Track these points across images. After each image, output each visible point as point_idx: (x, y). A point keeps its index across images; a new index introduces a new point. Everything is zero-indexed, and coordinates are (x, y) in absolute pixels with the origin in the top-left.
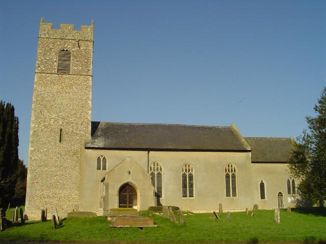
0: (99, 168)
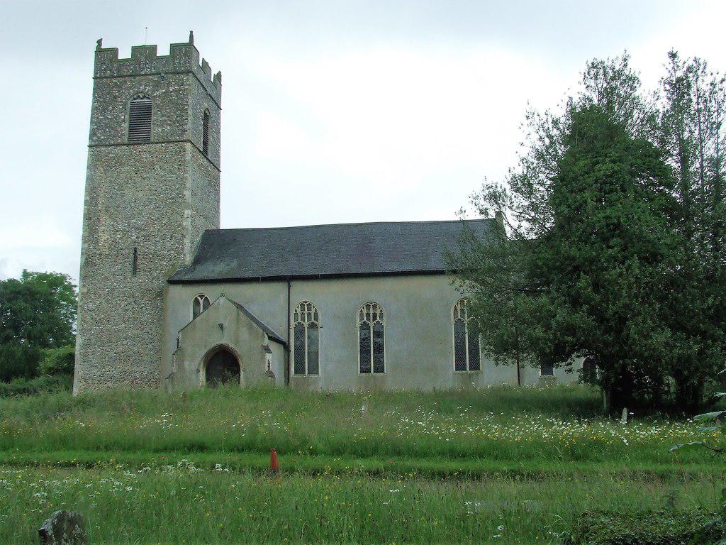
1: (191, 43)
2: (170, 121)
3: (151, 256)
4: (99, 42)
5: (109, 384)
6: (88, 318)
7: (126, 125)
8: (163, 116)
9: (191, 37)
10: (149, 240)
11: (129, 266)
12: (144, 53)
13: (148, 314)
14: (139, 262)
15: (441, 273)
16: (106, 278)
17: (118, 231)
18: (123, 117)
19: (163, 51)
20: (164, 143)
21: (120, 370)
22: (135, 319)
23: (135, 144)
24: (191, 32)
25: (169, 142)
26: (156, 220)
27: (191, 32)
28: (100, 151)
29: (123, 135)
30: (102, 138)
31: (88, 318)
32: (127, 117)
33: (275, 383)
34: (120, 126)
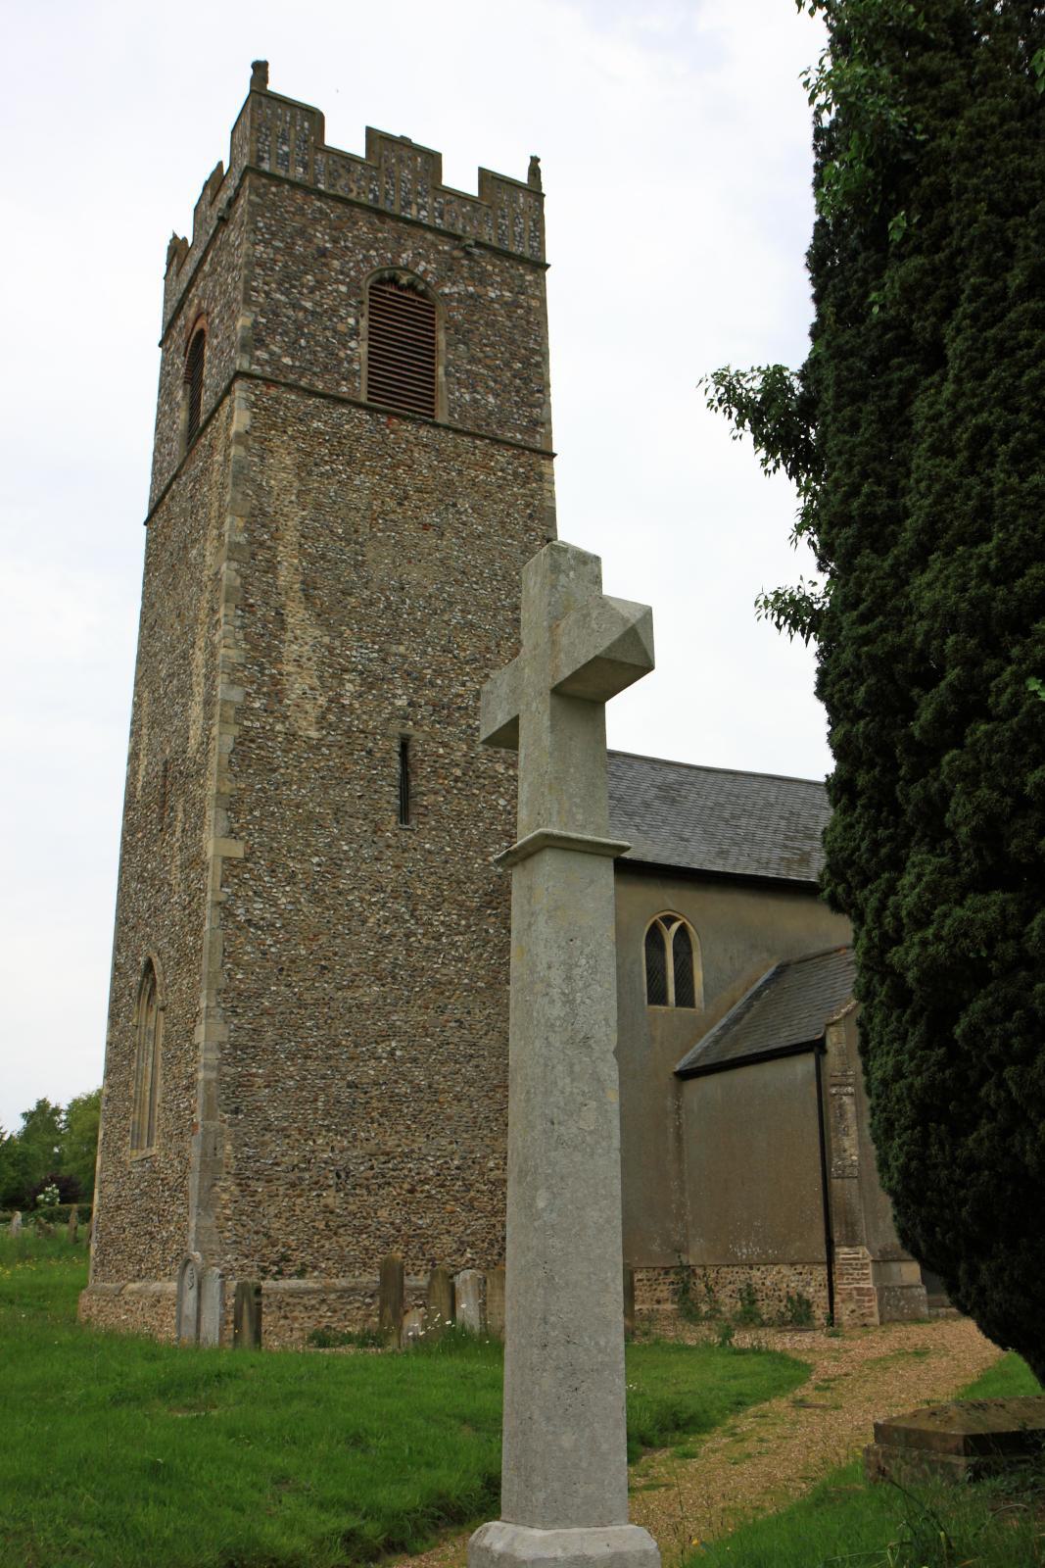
1: (533, 189)
2: (495, 381)
3: (458, 773)
4: (260, 69)
5: (331, 1198)
6: (249, 954)
7: (360, 348)
8: (473, 360)
9: (534, 170)
10: (448, 721)
11: (390, 794)
12: (399, 159)
13: (460, 959)
14: (417, 784)
15: (799, 962)
16: (311, 817)
17: (346, 671)
18: (351, 321)
19: (460, 177)
20: (482, 437)
21: (371, 1146)
22: (416, 972)
23: (397, 415)
24: (535, 160)
25: (496, 441)
26: (467, 663)
27: (535, 160)
28: (277, 400)
29: (355, 373)
30: (287, 360)
31: (249, 954)
32: (364, 323)
33: (458, 1273)
34: (345, 347)
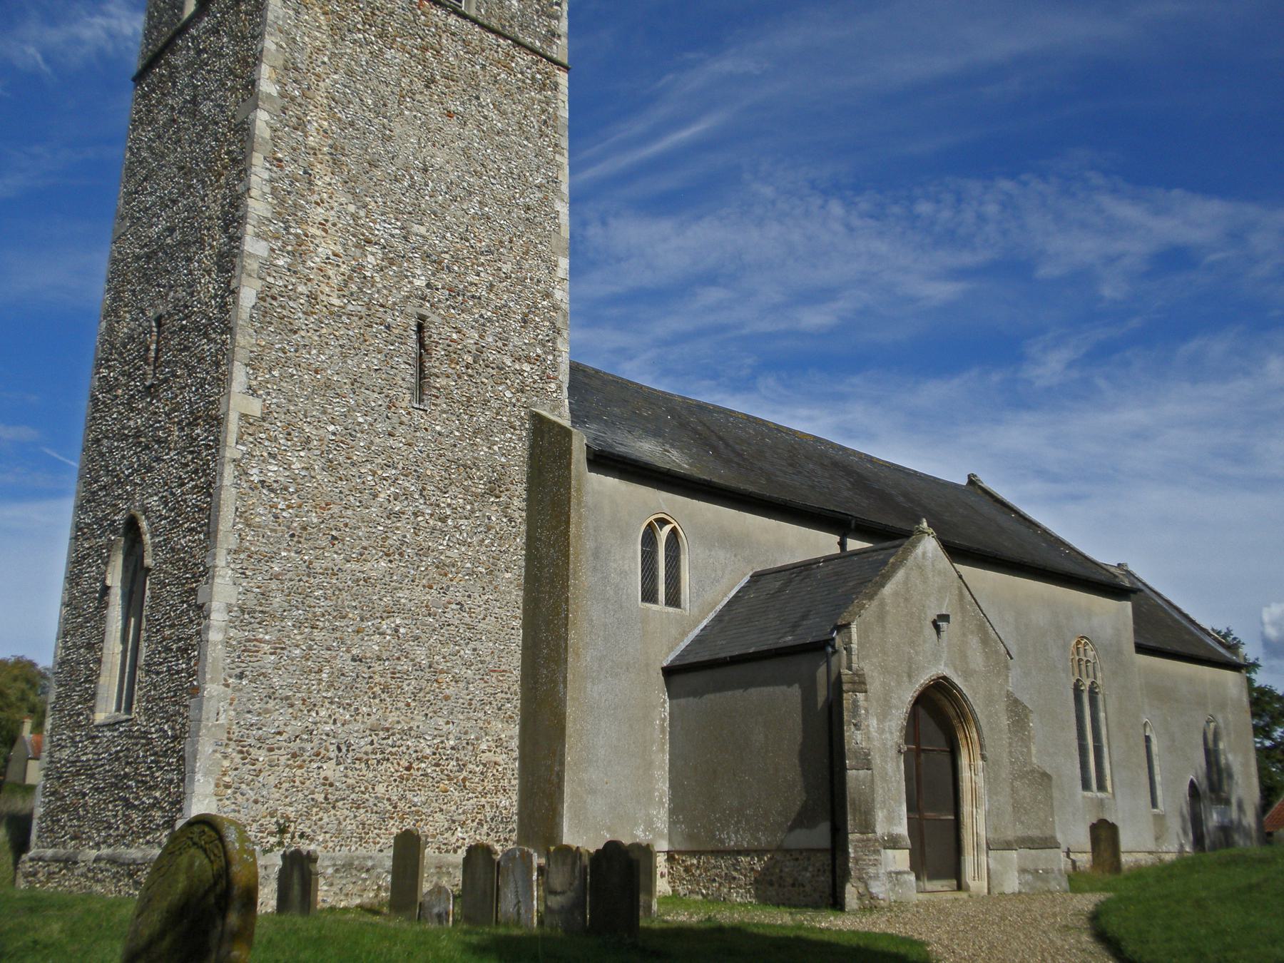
0: (649, 595)
11: (407, 373)
